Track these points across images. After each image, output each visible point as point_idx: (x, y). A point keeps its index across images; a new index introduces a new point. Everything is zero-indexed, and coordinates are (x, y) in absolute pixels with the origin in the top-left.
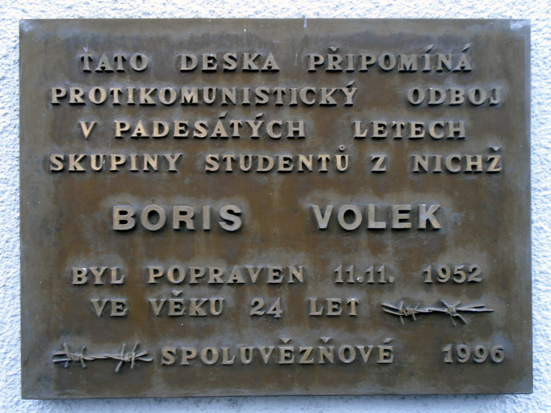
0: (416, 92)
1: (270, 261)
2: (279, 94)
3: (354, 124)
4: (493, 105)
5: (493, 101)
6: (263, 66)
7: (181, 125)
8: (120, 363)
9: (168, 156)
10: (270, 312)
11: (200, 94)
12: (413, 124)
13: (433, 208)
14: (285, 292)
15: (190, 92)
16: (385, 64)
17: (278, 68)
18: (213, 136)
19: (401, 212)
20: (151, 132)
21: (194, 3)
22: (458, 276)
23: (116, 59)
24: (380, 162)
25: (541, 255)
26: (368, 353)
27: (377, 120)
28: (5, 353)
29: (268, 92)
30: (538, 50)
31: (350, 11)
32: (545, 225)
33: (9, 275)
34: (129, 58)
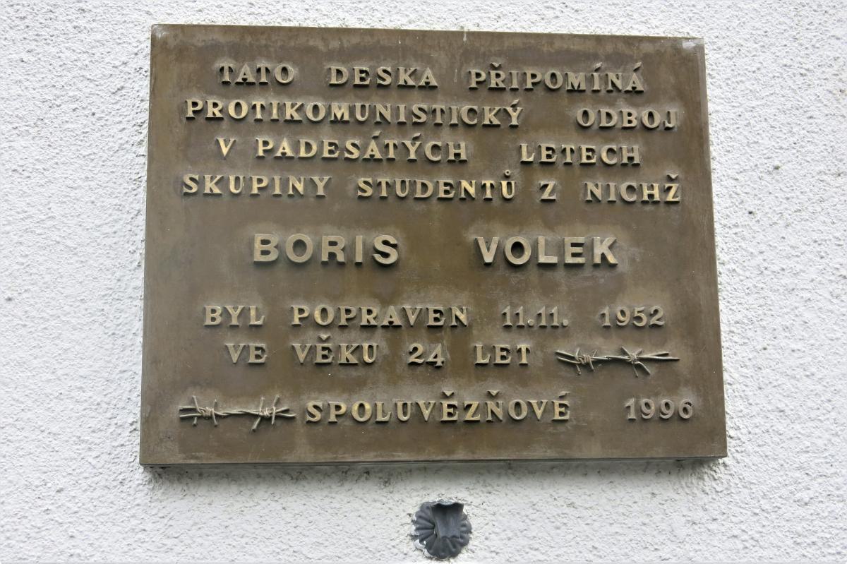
0: (585, 114)
1: (430, 301)
2: (438, 113)
3: (521, 146)
4: (668, 129)
5: (668, 125)
6: (420, 82)
7: (331, 144)
8: (259, 420)
9: (316, 179)
10: (431, 359)
11: (352, 111)
12: (584, 148)
13: (609, 241)
14: (446, 336)
15: (340, 108)
16: (552, 82)
17: (436, 84)
18: (365, 157)
19: (574, 245)
20: (297, 150)
21: (341, 10)
22: (639, 319)
23: (259, 70)
24: (549, 189)
25: (735, 302)
26: (542, 408)
27: (546, 143)
28: (110, 419)
29: (426, 110)
30: (720, 71)
31: (513, 23)
32: (738, 267)
33: (120, 321)
34: (274, 69)
